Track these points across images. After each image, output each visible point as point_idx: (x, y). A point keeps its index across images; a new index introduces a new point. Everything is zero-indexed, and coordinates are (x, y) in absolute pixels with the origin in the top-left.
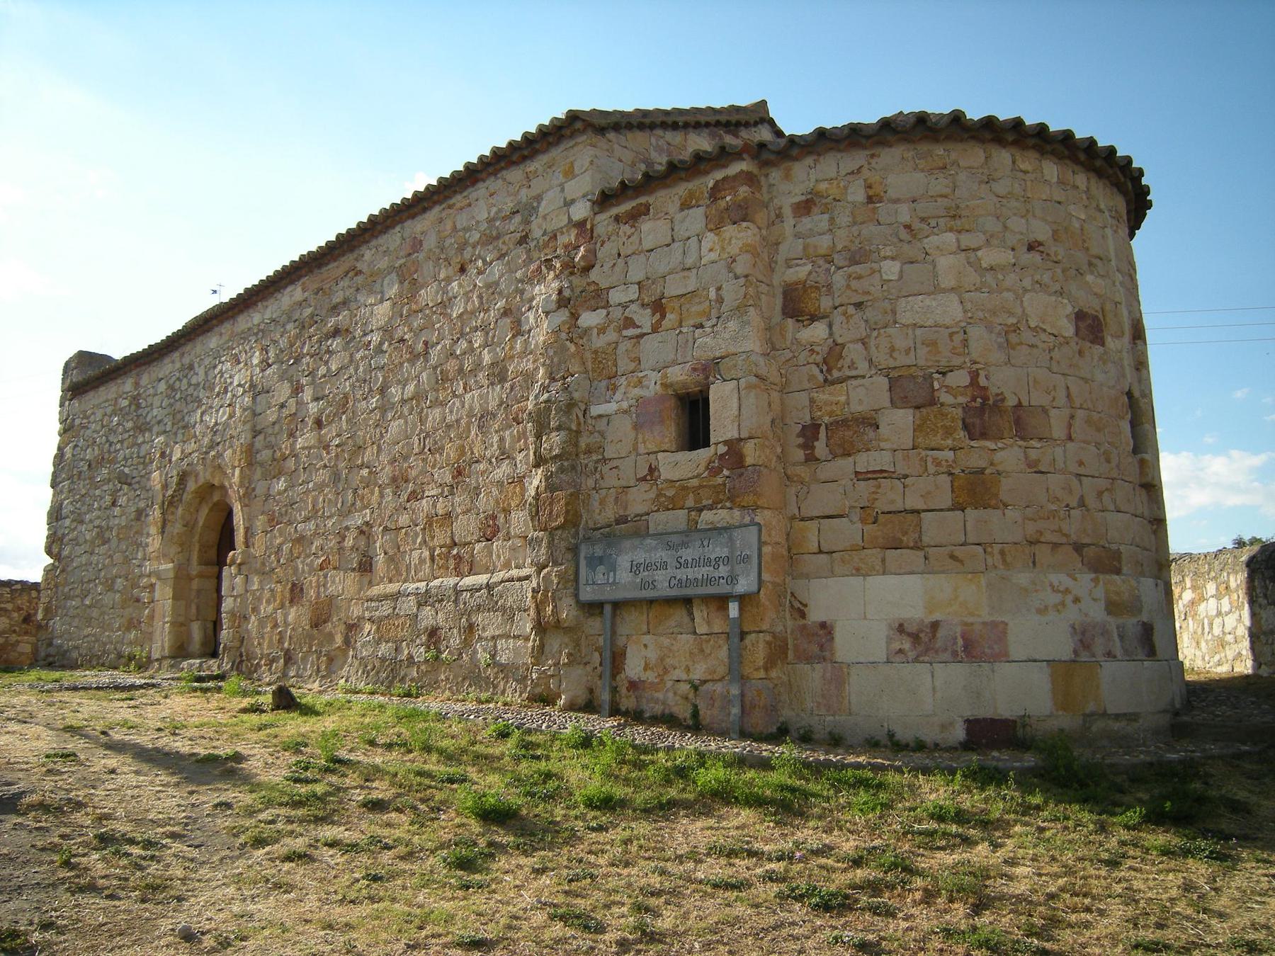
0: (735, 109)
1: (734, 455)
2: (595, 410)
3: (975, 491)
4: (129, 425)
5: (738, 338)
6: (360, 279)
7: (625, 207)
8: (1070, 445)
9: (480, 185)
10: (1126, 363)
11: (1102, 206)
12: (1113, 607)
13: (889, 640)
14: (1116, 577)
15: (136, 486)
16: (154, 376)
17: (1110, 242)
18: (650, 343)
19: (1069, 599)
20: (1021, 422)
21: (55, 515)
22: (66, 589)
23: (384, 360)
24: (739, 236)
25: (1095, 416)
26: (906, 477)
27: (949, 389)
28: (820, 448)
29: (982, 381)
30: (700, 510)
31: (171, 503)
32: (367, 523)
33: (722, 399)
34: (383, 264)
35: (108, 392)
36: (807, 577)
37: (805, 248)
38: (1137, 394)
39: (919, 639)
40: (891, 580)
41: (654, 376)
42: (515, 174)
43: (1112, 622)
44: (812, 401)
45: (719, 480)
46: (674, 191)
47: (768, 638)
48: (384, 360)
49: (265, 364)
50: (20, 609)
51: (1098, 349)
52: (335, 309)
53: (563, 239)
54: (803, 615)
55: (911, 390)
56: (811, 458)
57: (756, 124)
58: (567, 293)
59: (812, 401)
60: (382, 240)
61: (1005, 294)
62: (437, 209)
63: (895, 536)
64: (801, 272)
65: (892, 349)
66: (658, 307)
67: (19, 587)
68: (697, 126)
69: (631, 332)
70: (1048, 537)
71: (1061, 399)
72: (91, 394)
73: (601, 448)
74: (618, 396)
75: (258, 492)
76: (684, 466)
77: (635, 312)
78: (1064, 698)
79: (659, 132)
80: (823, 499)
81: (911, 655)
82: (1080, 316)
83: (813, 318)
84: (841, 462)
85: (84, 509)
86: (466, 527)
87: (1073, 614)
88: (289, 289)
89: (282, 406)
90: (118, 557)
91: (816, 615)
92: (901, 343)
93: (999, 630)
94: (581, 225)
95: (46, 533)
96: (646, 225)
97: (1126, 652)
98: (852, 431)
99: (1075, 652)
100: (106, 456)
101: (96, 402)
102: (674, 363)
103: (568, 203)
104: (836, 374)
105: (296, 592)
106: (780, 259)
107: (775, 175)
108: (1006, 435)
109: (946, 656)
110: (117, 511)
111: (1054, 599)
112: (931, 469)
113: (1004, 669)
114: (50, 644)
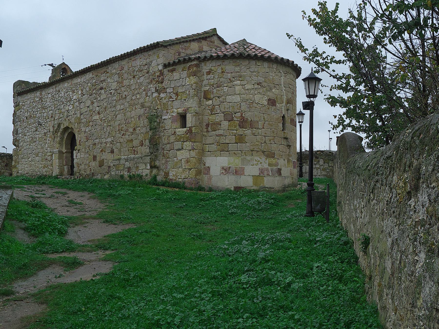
0: (205, 32)
1: (190, 131)
2: (163, 118)
3: (240, 139)
5: (192, 104)
7: (171, 68)
8: (263, 129)
9: (138, 55)
10: (283, 110)
11: (281, 72)
12: (270, 165)
13: (221, 170)
15: (44, 126)
16: (46, 92)
18: (176, 103)
20: (252, 125)
22: (22, 156)
23: (115, 98)
24: (193, 79)
27: (236, 117)
29: (243, 115)
31: (56, 132)
32: (112, 141)
33: (189, 116)
34: (114, 71)
35: (30, 96)
36: (206, 157)
38: (286, 116)
39: (226, 170)
40: (222, 158)
41: (176, 110)
42: (146, 54)
43: (270, 168)
44: (208, 118)
45: (188, 136)
46: (181, 66)
47: (196, 169)
48: (115, 98)
49: (83, 95)
53: (157, 74)
54: (205, 165)
55: (229, 117)
56: (208, 131)
57: (212, 36)
58: (157, 88)
59: (208, 118)
60: (113, 65)
61: (250, 95)
62: (127, 59)
63: (223, 149)
64: (207, 88)
65: (225, 108)
66: (177, 94)
67: (3, 155)
68: (194, 40)
69: (171, 100)
72: (25, 95)
73: (165, 127)
74: (168, 115)
75: (82, 130)
76: (181, 131)
78: (255, 184)
79: (182, 44)
80: (210, 140)
81: (225, 174)
82: (269, 100)
83: (210, 99)
84: (213, 132)
85: (26, 132)
86: (136, 143)
87: (260, 166)
88: (88, 73)
89: (88, 107)
90: (39, 147)
91: (207, 165)
92: (227, 107)
93: (243, 169)
94: (160, 71)
96: (175, 74)
98: (216, 125)
100: (32, 116)
102: (180, 108)
103: (158, 65)
104: (213, 112)
105: (95, 158)
106: (204, 84)
107: (203, 64)
110: (38, 133)
111: (255, 163)
113: (243, 177)
114: (18, 173)
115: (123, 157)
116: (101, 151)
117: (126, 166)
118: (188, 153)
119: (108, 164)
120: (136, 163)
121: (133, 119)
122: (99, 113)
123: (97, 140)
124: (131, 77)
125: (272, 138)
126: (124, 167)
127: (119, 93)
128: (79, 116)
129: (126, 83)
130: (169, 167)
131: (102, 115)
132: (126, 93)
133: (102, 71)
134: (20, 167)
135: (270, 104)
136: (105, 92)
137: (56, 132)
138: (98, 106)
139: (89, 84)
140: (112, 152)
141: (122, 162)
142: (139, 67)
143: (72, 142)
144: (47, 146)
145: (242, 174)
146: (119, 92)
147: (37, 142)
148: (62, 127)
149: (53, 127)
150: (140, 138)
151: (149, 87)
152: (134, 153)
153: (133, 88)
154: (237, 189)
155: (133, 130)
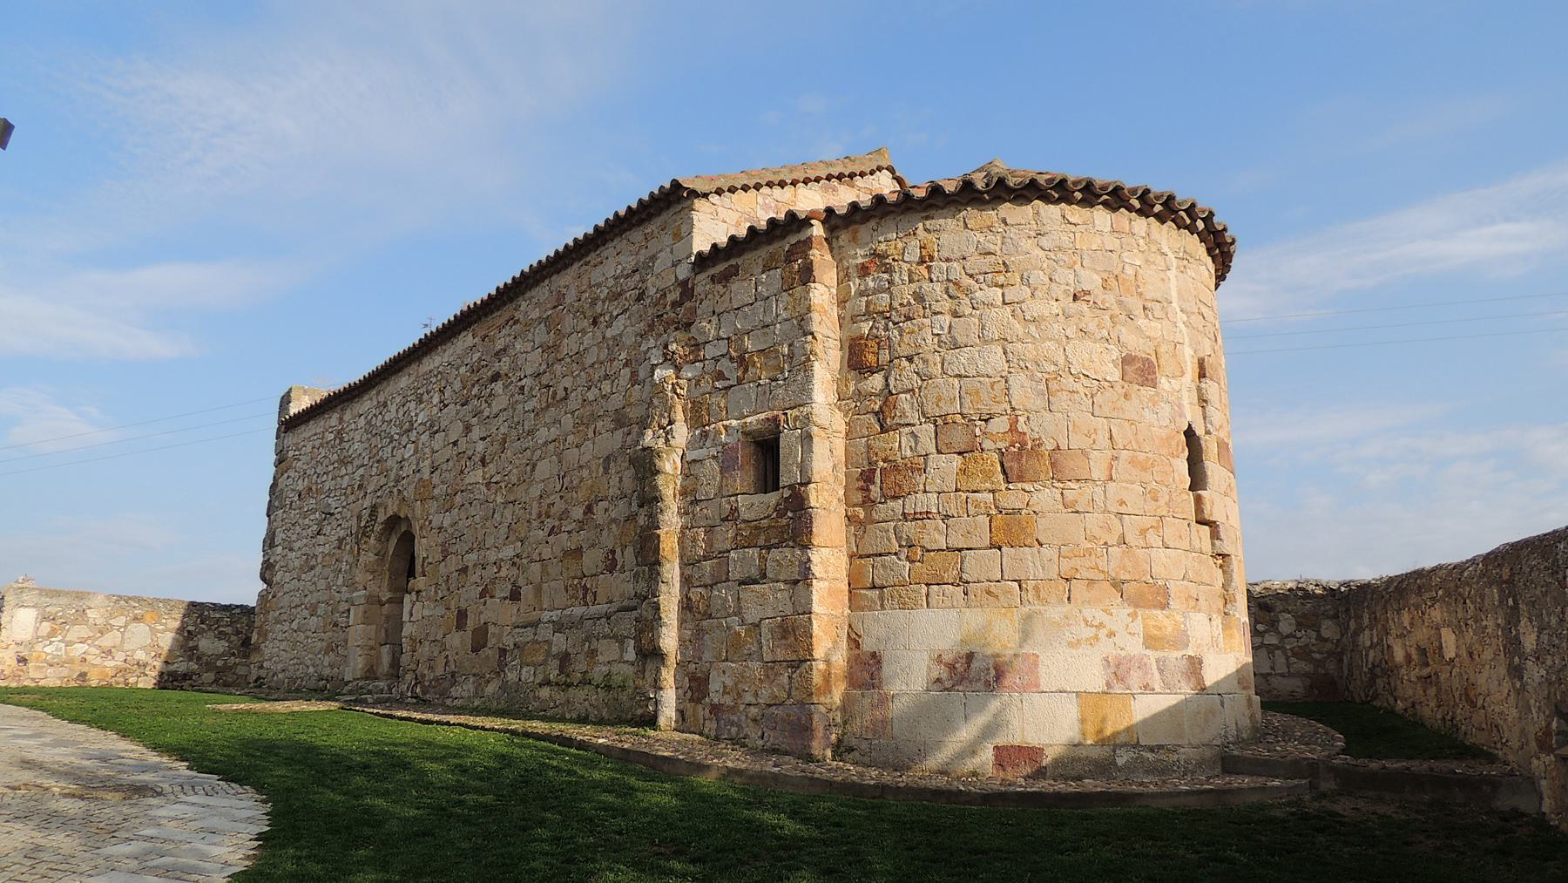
4: (335, 457)
6: (518, 326)
7: (721, 267)
8: (1111, 485)
9: (610, 244)
10: (1185, 402)
11: (1165, 249)
12: (1151, 641)
14: (1158, 612)
17: (1173, 284)
19: (1104, 631)
21: (269, 542)
25: (1142, 456)
26: (948, 517)
28: (875, 491)
29: (1022, 427)
30: (769, 548)
31: (364, 534)
34: (535, 314)
37: (868, 304)
38: (1199, 431)
42: (636, 235)
43: (1153, 655)
44: (869, 447)
45: (784, 521)
46: (758, 253)
50: (238, 633)
51: (1147, 392)
52: (498, 355)
53: (670, 298)
54: (858, 646)
59: (869, 447)
60: (534, 292)
62: (576, 266)
66: (743, 362)
70: (1085, 574)
71: (1103, 440)
77: (724, 365)
82: (1127, 360)
84: (891, 504)
85: (294, 537)
86: (592, 559)
87: (1106, 648)
89: (455, 444)
90: (322, 584)
91: (868, 645)
94: (683, 284)
95: (261, 560)
97: (1166, 685)
99: (1108, 684)
101: (306, 435)
105: (462, 615)
108: (1042, 476)
109: (980, 685)
110: (321, 539)
112: (972, 510)
114: (261, 667)
115: (546, 616)
116: (482, 595)
117: (554, 650)
118: (786, 594)
119: (499, 640)
120: (588, 639)
121: (585, 473)
122: (483, 462)
123: (473, 556)
124: (585, 323)
125: (1152, 521)
126: (548, 653)
127: (548, 387)
128: (426, 477)
129: (569, 345)
130: (707, 656)
131: (491, 468)
132: (567, 382)
133: (502, 321)
134: (268, 649)
135: (1131, 375)
136: (506, 387)
137: (364, 533)
138: (483, 439)
139: (463, 370)
140: (515, 596)
141: (545, 632)
142: (611, 282)
143: (405, 566)
144: (340, 582)
145: (1024, 689)
146: (545, 382)
147: (318, 569)
148: (382, 517)
149: (359, 518)
150: (607, 540)
151: (644, 348)
152: (585, 597)
153: (589, 361)
154: (657, 499)
155: (585, 513)
